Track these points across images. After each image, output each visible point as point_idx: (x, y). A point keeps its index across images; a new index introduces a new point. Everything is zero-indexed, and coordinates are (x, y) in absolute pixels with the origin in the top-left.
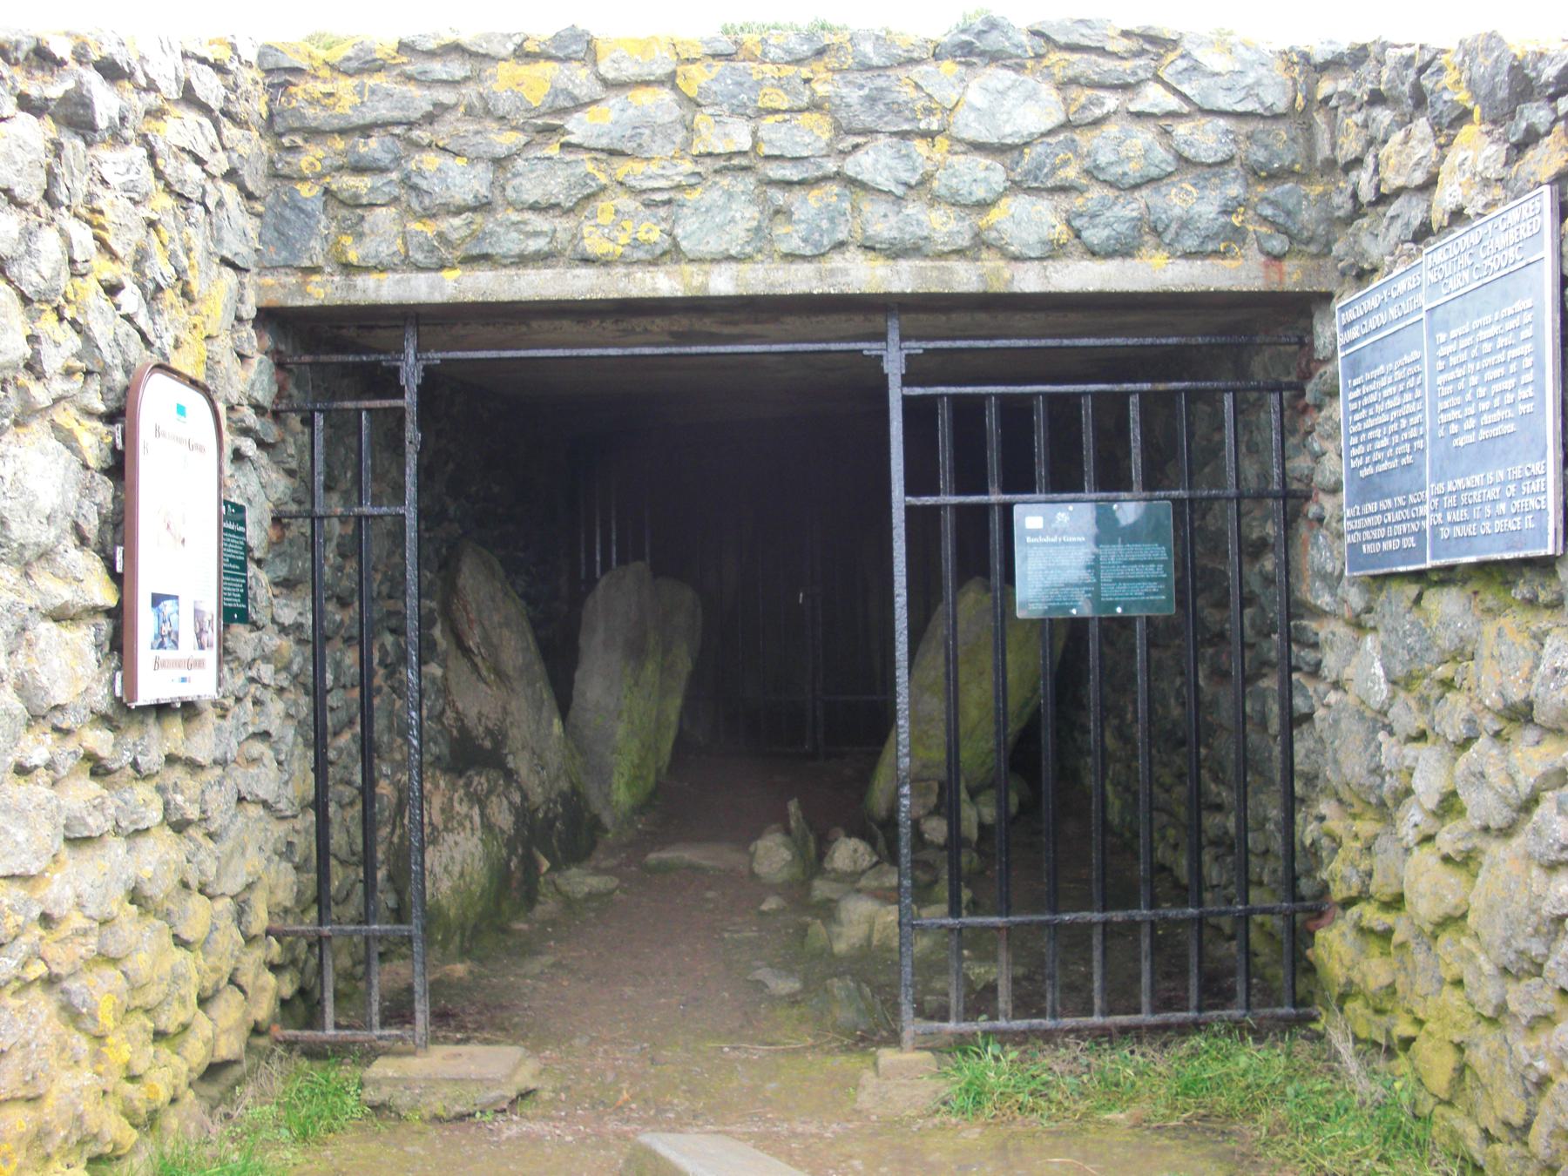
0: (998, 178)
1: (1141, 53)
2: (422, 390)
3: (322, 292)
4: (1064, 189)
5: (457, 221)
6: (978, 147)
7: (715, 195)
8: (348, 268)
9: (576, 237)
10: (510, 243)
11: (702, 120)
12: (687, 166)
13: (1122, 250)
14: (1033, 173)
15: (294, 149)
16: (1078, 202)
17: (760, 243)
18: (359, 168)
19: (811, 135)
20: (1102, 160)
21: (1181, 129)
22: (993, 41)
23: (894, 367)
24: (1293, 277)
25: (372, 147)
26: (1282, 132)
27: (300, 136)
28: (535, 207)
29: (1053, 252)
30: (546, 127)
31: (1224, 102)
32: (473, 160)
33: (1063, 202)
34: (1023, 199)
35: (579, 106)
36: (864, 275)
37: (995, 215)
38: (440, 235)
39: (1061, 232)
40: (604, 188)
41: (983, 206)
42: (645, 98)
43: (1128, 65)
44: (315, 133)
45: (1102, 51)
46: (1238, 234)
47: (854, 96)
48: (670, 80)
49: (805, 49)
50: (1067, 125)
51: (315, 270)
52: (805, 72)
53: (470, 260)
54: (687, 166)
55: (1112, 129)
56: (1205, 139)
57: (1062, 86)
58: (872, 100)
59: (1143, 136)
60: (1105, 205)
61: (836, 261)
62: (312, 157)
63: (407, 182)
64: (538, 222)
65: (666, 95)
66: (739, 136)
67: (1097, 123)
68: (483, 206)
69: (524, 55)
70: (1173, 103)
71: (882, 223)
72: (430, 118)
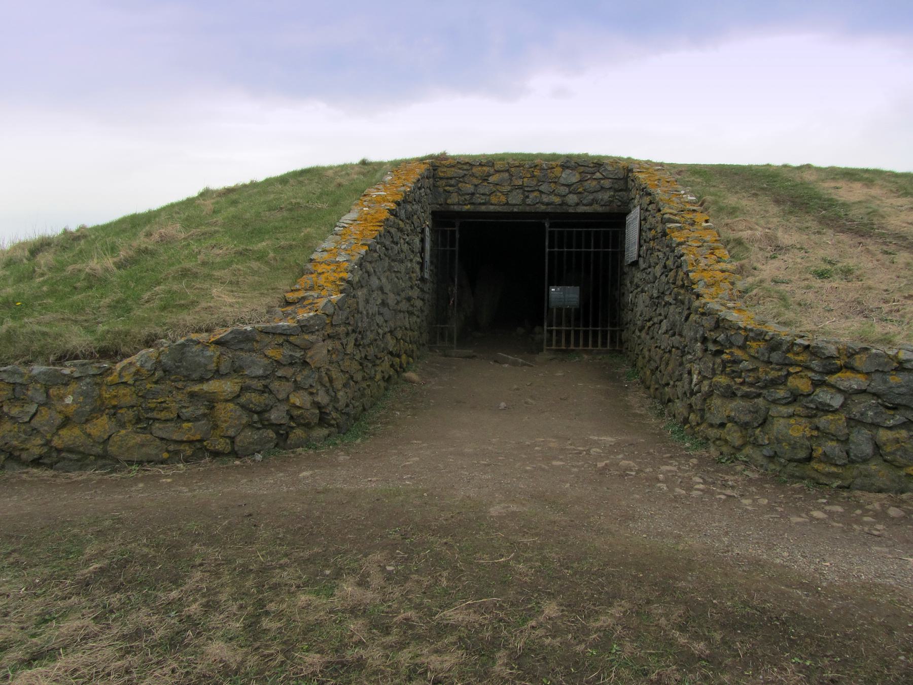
0: (567, 191)
6: (563, 185)
10: (479, 201)
13: (590, 204)
18: (450, 186)
22: (568, 164)
23: (547, 225)
25: (453, 182)
26: (622, 182)
31: (611, 176)
48: (507, 171)
56: (607, 183)
57: (580, 173)
59: (594, 183)
63: (459, 189)
64: (483, 197)
68: (473, 194)
69: (481, 165)
70: (601, 176)
71: (545, 199)
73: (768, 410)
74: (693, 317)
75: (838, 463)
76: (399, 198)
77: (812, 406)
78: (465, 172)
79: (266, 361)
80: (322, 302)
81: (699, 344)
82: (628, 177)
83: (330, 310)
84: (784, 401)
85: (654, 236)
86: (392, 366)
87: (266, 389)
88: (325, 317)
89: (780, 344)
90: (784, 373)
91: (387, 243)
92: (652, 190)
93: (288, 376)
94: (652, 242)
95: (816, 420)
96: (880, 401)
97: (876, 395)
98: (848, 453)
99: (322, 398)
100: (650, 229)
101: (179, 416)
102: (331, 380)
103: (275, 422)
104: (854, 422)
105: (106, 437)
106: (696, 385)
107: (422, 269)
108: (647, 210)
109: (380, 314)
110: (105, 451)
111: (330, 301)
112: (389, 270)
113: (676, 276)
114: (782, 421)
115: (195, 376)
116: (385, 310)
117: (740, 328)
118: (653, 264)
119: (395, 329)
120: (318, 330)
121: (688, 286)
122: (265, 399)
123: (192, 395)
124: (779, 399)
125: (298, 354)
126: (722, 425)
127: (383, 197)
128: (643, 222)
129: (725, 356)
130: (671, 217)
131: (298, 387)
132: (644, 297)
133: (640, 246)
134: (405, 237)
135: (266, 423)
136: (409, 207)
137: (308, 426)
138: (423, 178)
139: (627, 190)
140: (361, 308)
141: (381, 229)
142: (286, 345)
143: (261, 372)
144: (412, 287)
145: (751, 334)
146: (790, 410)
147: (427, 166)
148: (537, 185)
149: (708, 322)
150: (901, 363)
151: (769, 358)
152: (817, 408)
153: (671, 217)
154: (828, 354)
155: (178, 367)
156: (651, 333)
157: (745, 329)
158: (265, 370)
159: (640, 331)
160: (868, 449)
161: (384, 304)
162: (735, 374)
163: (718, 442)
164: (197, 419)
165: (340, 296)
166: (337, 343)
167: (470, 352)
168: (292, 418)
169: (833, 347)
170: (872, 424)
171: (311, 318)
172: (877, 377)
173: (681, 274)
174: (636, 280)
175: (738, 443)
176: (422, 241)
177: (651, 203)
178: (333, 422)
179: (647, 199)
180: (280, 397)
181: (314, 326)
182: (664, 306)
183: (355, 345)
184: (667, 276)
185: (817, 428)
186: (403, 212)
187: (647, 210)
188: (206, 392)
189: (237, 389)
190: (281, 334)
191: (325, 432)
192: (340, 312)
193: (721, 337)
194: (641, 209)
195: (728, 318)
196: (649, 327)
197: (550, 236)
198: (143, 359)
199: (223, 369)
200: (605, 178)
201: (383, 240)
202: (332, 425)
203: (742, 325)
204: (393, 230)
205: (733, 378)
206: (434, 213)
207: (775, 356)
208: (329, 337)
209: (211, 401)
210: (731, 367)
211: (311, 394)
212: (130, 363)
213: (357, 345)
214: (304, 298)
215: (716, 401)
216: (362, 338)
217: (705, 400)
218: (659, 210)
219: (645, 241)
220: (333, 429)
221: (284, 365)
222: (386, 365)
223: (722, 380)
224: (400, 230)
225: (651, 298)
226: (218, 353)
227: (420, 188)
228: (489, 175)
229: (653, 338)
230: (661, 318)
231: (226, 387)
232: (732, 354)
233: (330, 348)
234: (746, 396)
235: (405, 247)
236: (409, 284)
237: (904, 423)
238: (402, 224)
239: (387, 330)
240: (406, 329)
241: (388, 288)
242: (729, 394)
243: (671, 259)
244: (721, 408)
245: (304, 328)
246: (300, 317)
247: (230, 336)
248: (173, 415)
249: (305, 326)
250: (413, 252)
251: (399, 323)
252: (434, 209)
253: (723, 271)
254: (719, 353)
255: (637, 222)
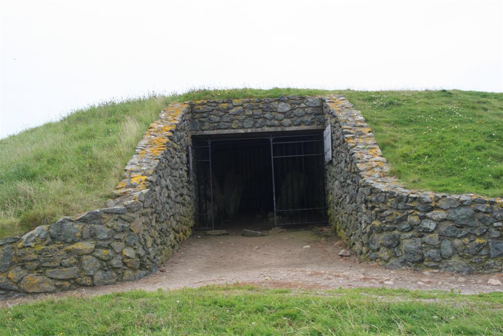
0: (283, 117)
1: (300, 99)
2: (211, 145)
3: (199, 133)
4: (291, 118)
5: (216, 124)
7: (248, 120)
8: (203, 130)
9: (231, 126)
10: (223, 127)
11: (246, 110)
12: (244, 116)
13: (299, 125)
14: (287, 116)
15: (195, 115)
16: (293, 119)
17: (254, 126)
18: (203, 117)
19: (259, 112)
20: (296, 114)
21: (306, 109)
23: (271, 140)
24: (320, 127)
25: (205, 115)
26: (319, 109)
27: (200, 107)
28: (226, 122)
29: (290, 125)
30: (226, 111)
31: (312, 105)
32: (218, 116)
33: (291, 119)
34: (286, 119)
35: (231, 109)
36: (267, 129)
37: (283, 121)
38: (214, 126)
39: (291, 123)
40: (234, 120)
41: (281, 120)
42: (238, 108)
43: (299, 101)
44: (197, 113)
45: (296, 100)
46: (314, 122)
47: (265, 107)
48: (242, 105)
49: (259, 101)
50: (291, 109)
51: (198, 130)
52: (259, 104)
53: (218, 129)
54: (244, 116)
55: (297, 110)
56: (309, 110)
57: (291, 104)
58: (267, 107)
59: (301, 111)
60: (296, 119)
61: (263, 128)
62: (197, 116)
63: (209, 119)
64: (226, 124)
65: (241, 107)
66: (251, 113)
67: (296, 109)
70: (305, 106)
71: (269, 123)
72: (212, 111)
73: (400, 236)
74: (360, 189)
75: (437, 260)
76: (173, 128)
77: (421, 230)
78: (213, 108)
79: (109, 230)
80: (137, 194)
81: (364, 205)
82: (323, 105)
83: (143, 199)
84: (407, 230)
85: (339, 144)
86: (175, 238)
87: (109, 247)
88: (140, 202)
89: (402, 198)
90: (405, 213)
91: (169, 158)
92: (336, 113)
93: (122, 238)
94: (338, 147)
95: (423, 239)
96: (454, 224)
97: (452, 221)
98: (441, 255)
99: (142, 252)
100: (337, 139)
101: (61, 265)
102: (145, 240)
103: (115, 266)
104: (442, 237)
105: (20, 279)
106: (364, 229)
107: (188, 175)
108: (334, 127)
109: (168, 203)
110: (19, 288)
111: (142, 193)
112: (171, 175)
113: (351, 167)
114: (407, 240)
115: (69, 240)
116: (169, 201)
117: (382, 192)
118: (340, 161)
119: (176, 214)
120: (136, 211)
121: (357, 172)
122: (109, 252)
123: (68, 252)
124: (404, 229)
125: (126, 225)
126: (378, 250)
127: (164, 126)
128: (333, 135)
129: (377, 209)
130: (348, 130)
131: (127, 245)
132: (337, 183)
133: (333, 150)
134: (178, 153)
135: (110, 267)
136: (178, 133)
137: (133, 269)
138: (185, 114)
139: (323, 114)
140: (158, 199)
141: (165, 149)
142: (120, 220)
143: (106, 236)
144: (183, 187)
145: (388, 194)
146: (410, 234)
147: (187, 106)
148: (262, 114)
149: (366, 191)
150: (462, 202)
151: (397, 207)
152: (423, 232)
153: (348, 130)
154: (426, 201)
155: (59, 235)
156: (342, 206)
157: (385, 192)
158: (108, 235)
159: (337, 206)
160: (450, 251)
161: (169, 197)
162: (381, 219)
163: (377, 260)
164: (71, 266)
165: (147, 190)
166: (147, 219)
167: (224, 231)
168: (125, 264)
169: (428, 197)
170: (451, 237)
171: (132, 203)
172: (451, 211)
173: (353, 164)
174: (332, 173)
175: (386, 257)
176: (187, 156)
177: (336, 122)
178: (148, 267)
179: (333, 120)
180: (117, 251)
181: (134, 208)
182: (347, 186)
183: (156, 221)
184: (347, 167)
185: (424, 243)
186: (176, 137)
187: (334, 127)
188: (76, 250)
189: (93, 246)
190: (116, 213)
191: (144, 272)
192: (148, 200)
193: (374, 199)
194: (331, 126)
195: (376, 187)
196: (341, 202)
197: (273, 148)
198: (39, 232)
199: (85, 236)
200: (308, 107)
201: (167, 156)
202: (147, 269)
203: (383, 190)
204: (171, 149)
205: (381, 221)
206: (193, 137)
207: (401, 206)
208: (143, 215)
209: (79, 256)
210: (379, 216)
211: (135, 249)
212: (32, 235)
213: (157, 222)
214: (125, 193)
215: (376, 236)
216: (160, 217)
217: (369, 236)
218: (341, 127)
219: (335, 148)
220: (148, 271)
221: (119, 232)
222: (172, 236)
223: (377, 223)
224: (175, 149)
225: (341, 182)
226: (81, 226)
227: (184, 121)
228: (229, 109)
229: (343, 208)
230: (346, 194)
231: (86, 246)
232: (379, 207)
233: (144, 222)
234: (389, 230)
235: (178, 160)
236: (181, 185)
237: (467, 234)
238: (175, 145)
239: (172, 214)
240: (181, 215)
241: (170, 187)
242: (381, 230)
243: (348, 157)
244: (380, 239)
245: (129, 209)
246: (126, 203)
247: (88, 216)
248: (57, 264)
249: (129, 208)
250: (182, 163)
251: (177, 210)
252: (193, 134)
253: (376, 161)
254: (373, 208)
255: (330, 135)
